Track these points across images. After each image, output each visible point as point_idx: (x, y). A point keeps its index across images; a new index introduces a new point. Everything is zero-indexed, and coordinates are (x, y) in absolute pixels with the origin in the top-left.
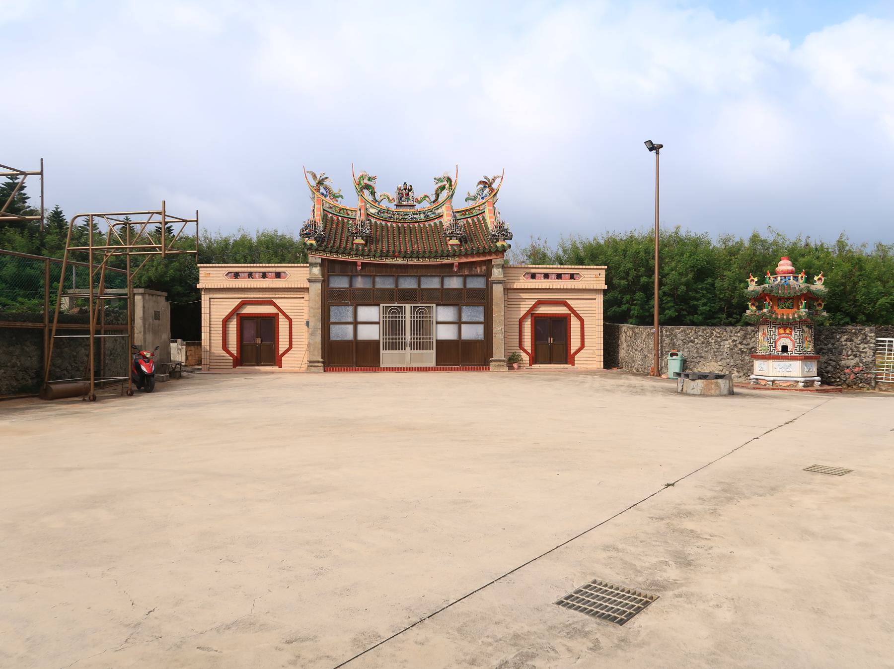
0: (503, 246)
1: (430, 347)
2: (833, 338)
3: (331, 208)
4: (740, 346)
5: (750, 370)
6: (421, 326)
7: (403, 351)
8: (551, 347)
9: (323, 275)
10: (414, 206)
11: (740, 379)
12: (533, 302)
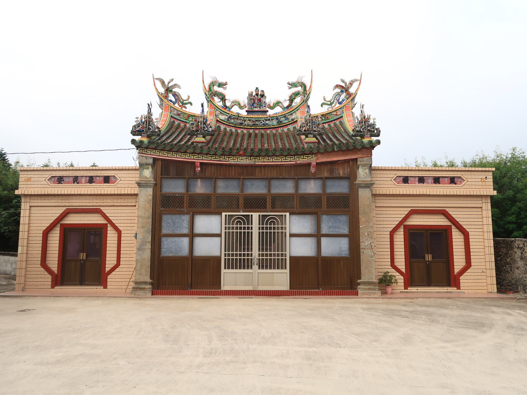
0: (371, 142)
1: (284, 267)
3: (179, 115)
6: (272, 240)
7: (249, 271)
8: (428, 266)
9: (155, 179)
10: (267, 111)
12: (406, 212)
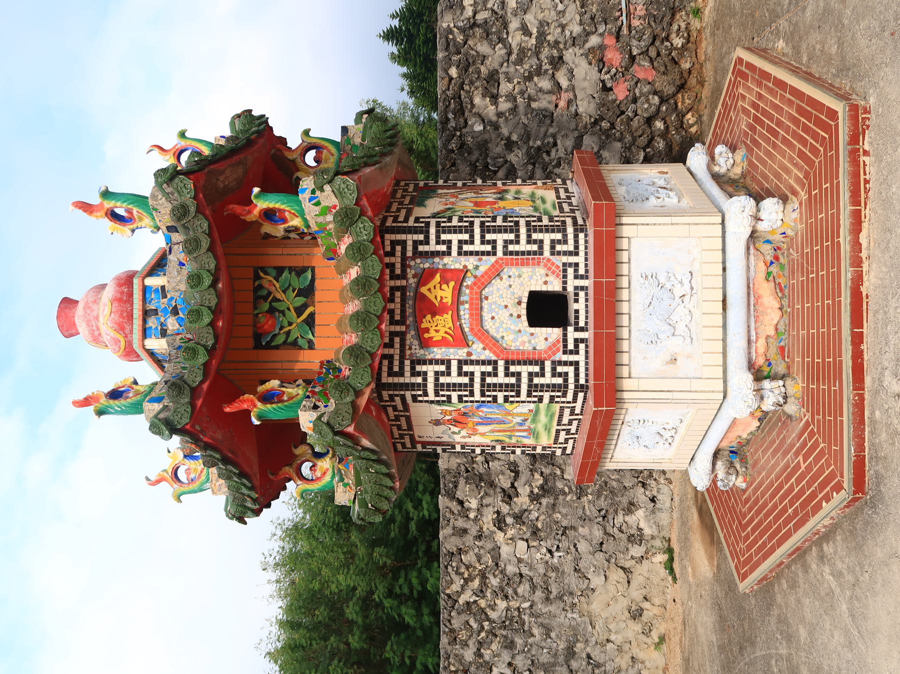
2: (483, 146)
4: (522, 501)
11: (664, 500)
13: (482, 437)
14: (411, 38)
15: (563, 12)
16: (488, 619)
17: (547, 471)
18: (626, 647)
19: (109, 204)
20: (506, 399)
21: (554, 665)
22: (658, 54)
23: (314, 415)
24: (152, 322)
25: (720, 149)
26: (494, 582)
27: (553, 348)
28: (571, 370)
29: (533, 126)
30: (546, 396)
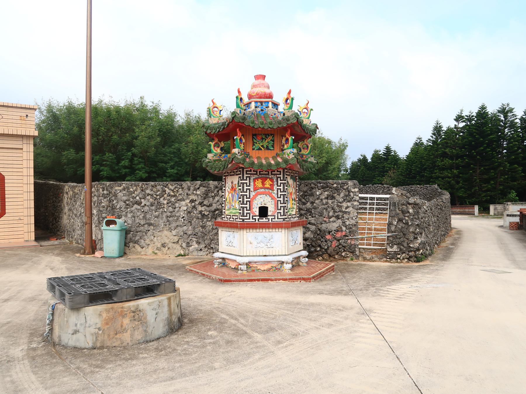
2: (312, 195)
4: (200, 208)
5: (212, 245)
11: (201, 253)
13: (228, 195)
14: (386, 159)
15: (353, 219)
16: (160, 198)
17: (209, 216)
18: (152, 242)
19: (290, 98)
20: (240, 201)
21: (146, 219)
22: (340, 248)
23: (237, 153)
24: (259, 104)
25: (307, 259)
26: (173, 199)
27: (253, 213)
28: (248, 218)
29: (318, 210)
30: (241, 212)
